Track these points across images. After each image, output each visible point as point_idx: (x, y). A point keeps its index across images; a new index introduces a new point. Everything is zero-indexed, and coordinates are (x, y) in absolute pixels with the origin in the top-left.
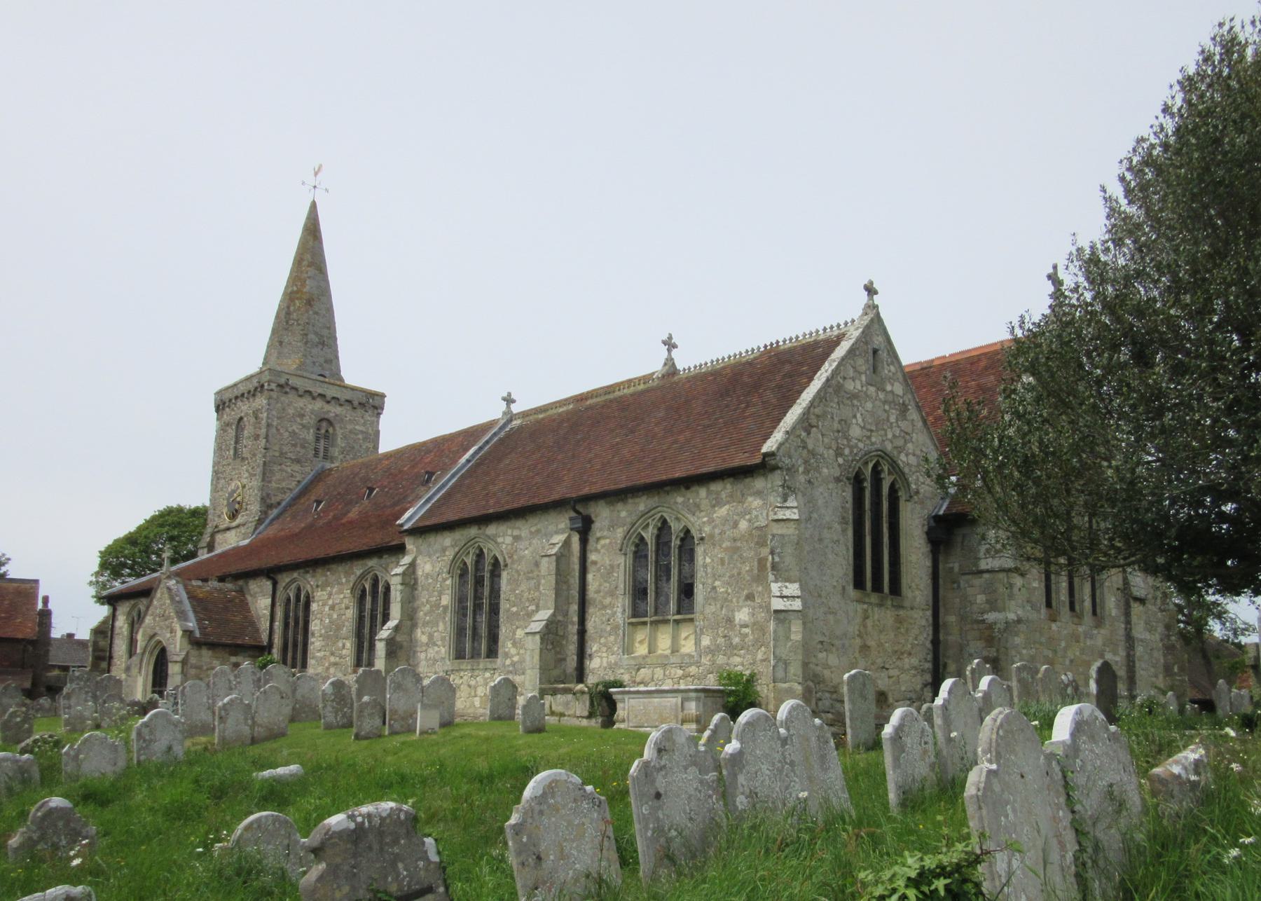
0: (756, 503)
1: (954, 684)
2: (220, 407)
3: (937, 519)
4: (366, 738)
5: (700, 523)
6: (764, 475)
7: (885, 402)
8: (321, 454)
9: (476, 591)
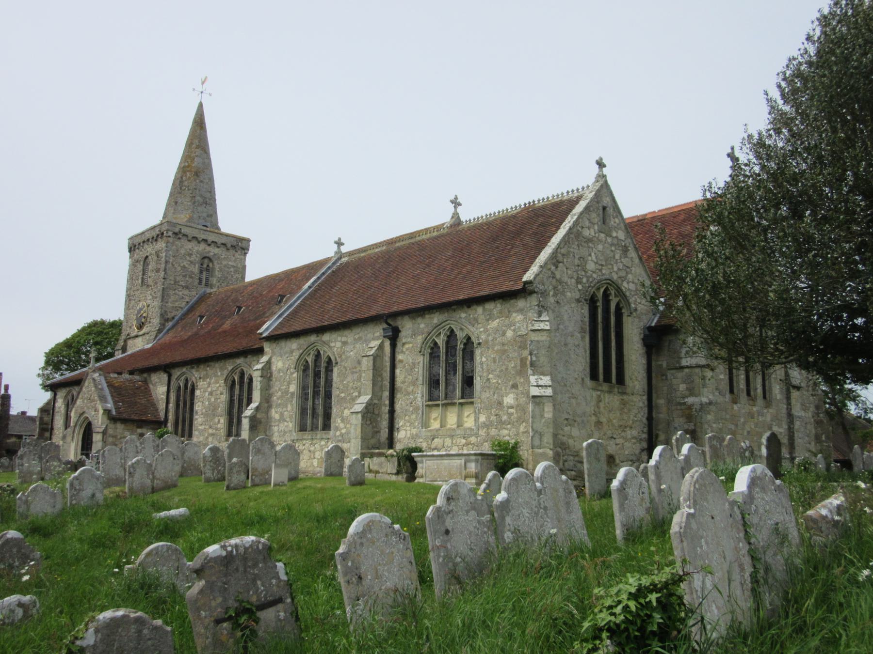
0: (518, 317)
1: (664, 450)
3: (650, 329)
4: (235, 489)
6: (525, 297)
7: (612, 245)
8: (204, 282)
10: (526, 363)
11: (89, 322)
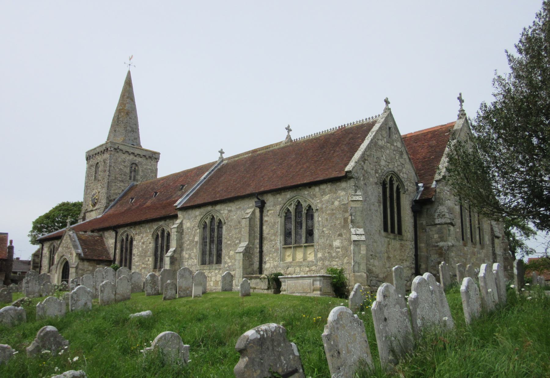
0: (343, 193)
2: (88, 158)
3: (416, 201)
4: (169, 299)
5: (316, 203)
6: (346, 181)
7: (394, 150)
8: (132, 178)
9: (211, 235)
10: (347, 221)
11: (60, 203)
